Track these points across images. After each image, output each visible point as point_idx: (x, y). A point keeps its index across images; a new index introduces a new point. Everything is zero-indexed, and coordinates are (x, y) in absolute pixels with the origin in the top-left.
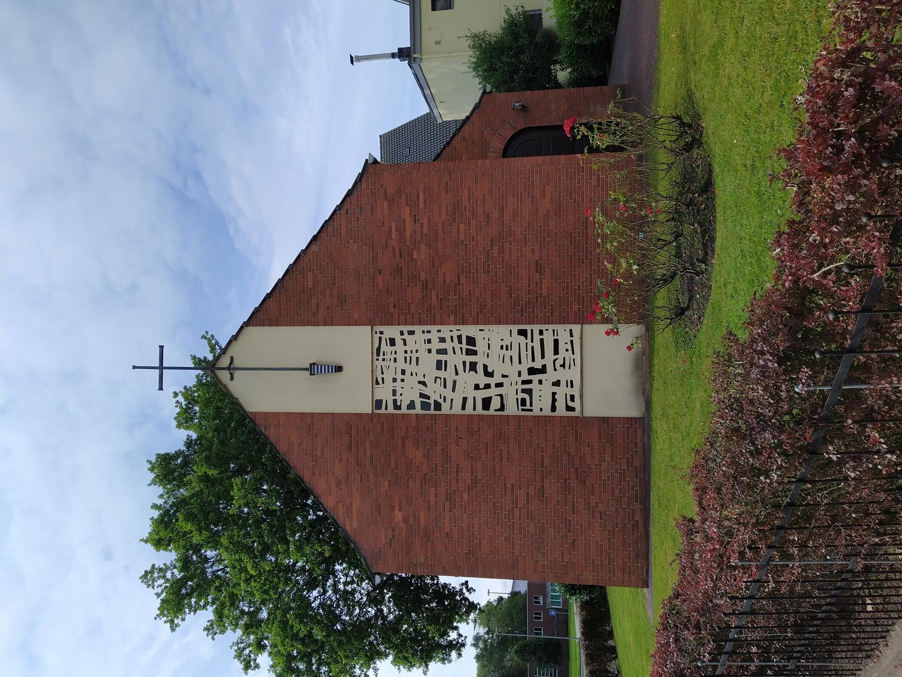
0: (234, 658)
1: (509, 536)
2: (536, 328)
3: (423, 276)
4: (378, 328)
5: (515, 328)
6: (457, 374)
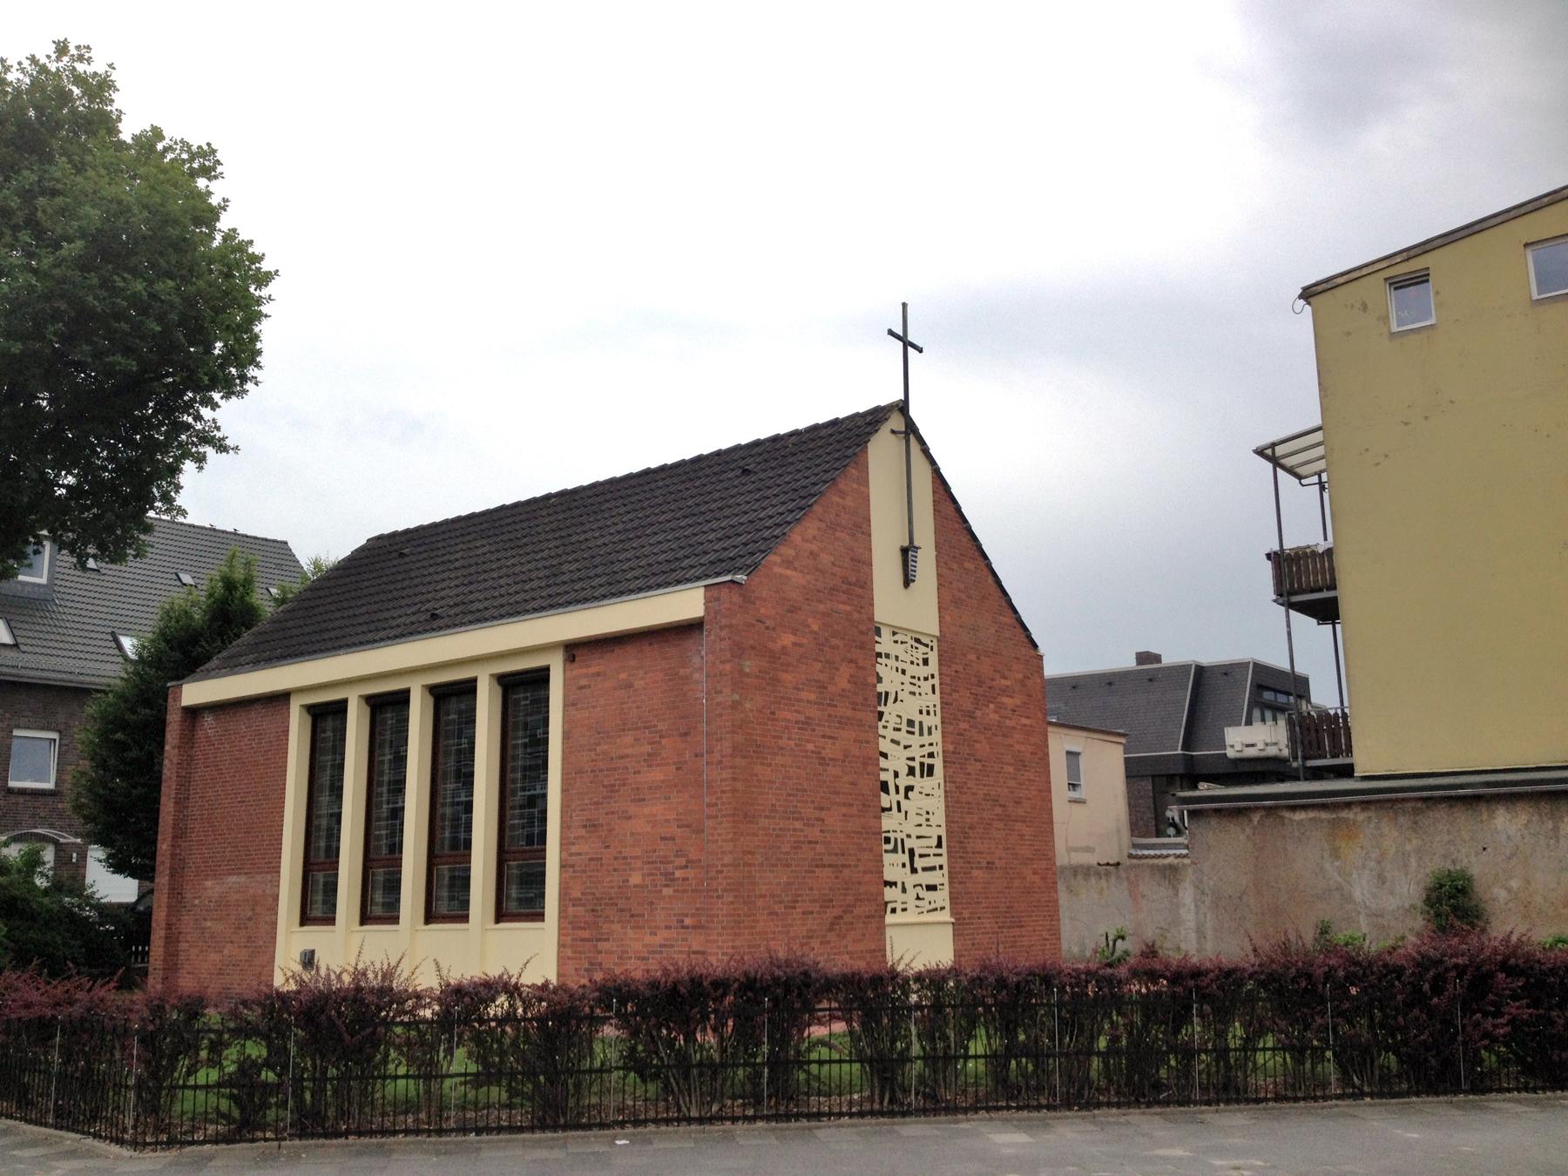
0: (263, 255)
1: (776, 811)
2: (943, 860)
3: (978, 713)
4: (935, 645)
5: (943, 832)
6: (906, 747)
